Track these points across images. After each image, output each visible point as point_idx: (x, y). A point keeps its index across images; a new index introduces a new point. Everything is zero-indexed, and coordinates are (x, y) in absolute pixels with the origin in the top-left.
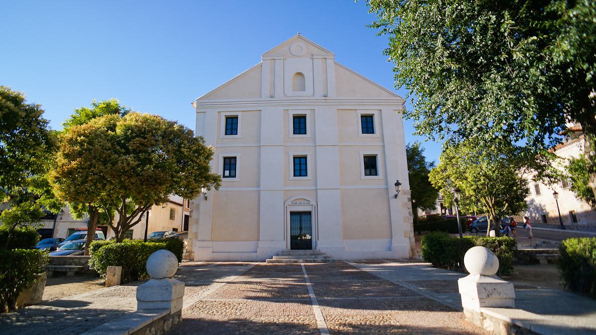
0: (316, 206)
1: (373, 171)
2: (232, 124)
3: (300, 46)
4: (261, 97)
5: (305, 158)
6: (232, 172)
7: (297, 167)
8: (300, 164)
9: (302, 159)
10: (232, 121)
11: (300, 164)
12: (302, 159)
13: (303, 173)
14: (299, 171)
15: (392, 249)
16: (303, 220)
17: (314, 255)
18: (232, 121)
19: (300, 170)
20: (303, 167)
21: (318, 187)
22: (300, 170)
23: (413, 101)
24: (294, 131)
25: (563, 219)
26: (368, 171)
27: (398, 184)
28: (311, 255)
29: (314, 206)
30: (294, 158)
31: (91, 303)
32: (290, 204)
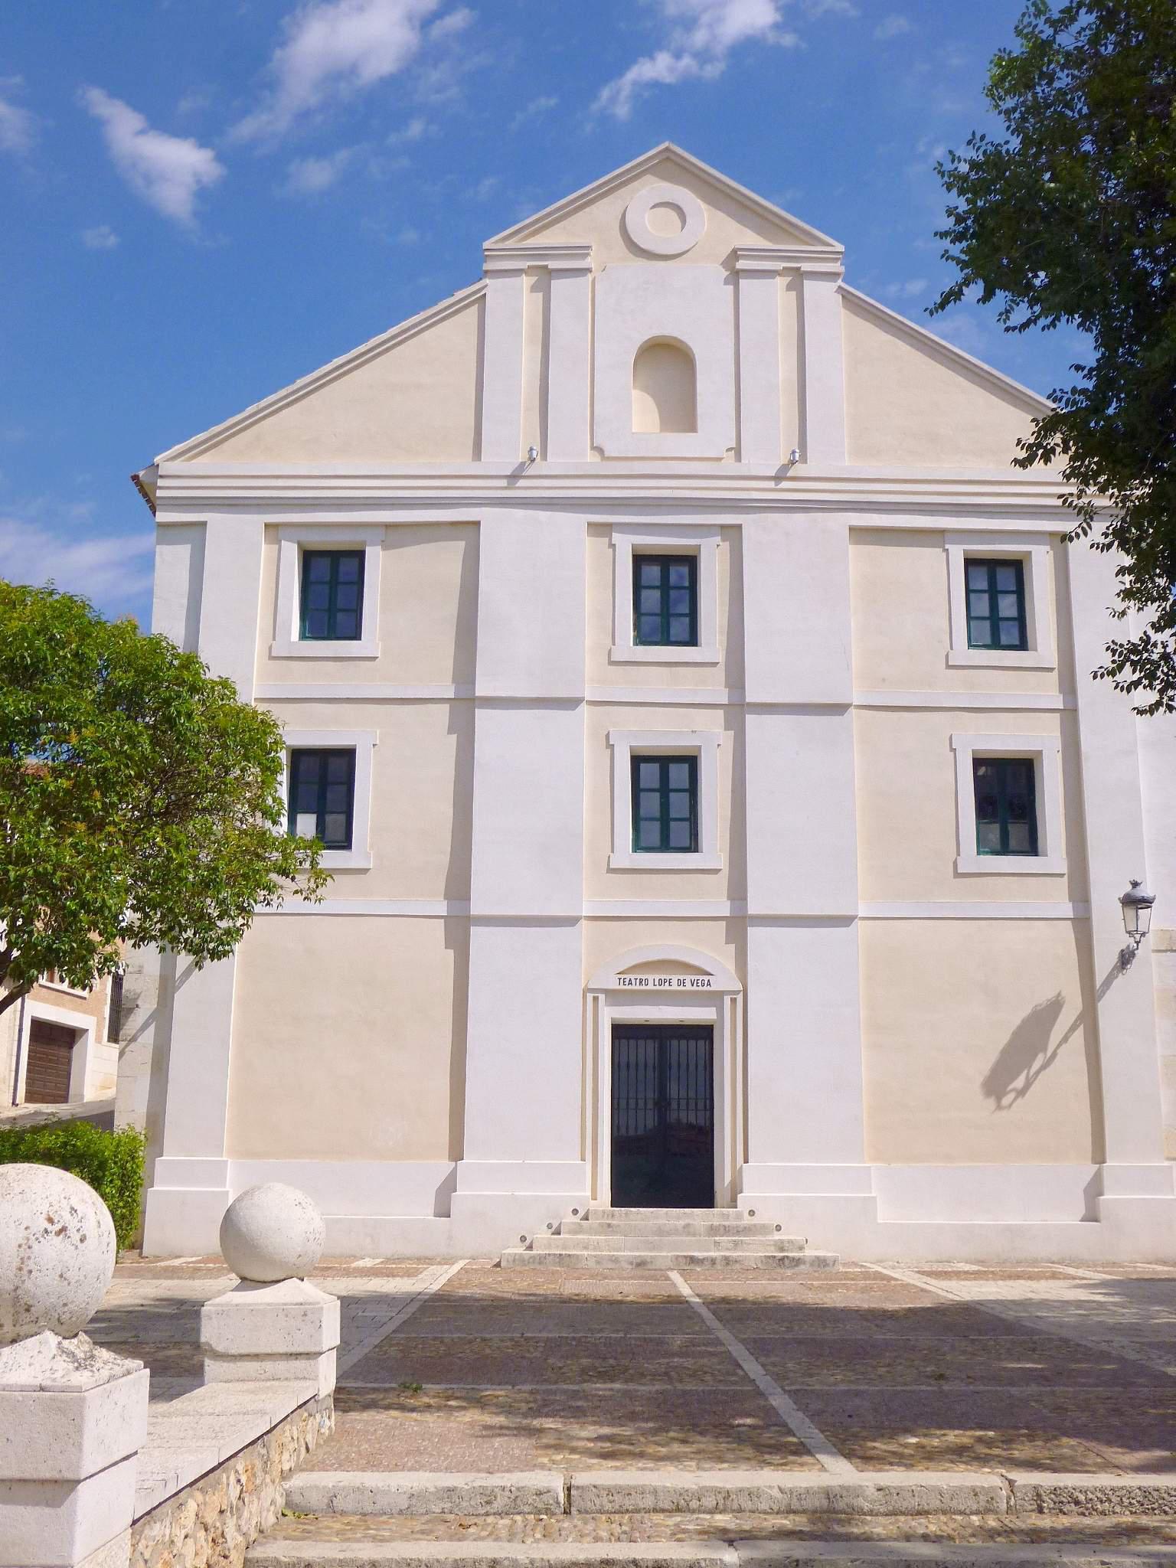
0: (740, 998)
1: (1017, 831)
2: (334, 583)
3: (636, 249)
4: (477, 453)
5: (691, 762)
6: (334, 820)
7: (652, 803)
8: (665, 790)
9: (673, 768)
10: (335, 570)
11: (665, 790)
12: (673, 768)
13: (678, 831)
14: (657, 825)
15: (1102, 1215)
16: (650, 1073)
17: (726, 1230)
18: (335, 570)
19: (665, 819)
20: (678, 803)
21: (754, 908)
22: (665, 819)
23: (73, 1247)
24: (637, 626)
25: (55, 1503)
26: (994, 832)
27: (1135, 902)
28: (713, 1230)
29: (727, 999)
30: (638, 761)
31: (683, 228)
32: (614, 985)
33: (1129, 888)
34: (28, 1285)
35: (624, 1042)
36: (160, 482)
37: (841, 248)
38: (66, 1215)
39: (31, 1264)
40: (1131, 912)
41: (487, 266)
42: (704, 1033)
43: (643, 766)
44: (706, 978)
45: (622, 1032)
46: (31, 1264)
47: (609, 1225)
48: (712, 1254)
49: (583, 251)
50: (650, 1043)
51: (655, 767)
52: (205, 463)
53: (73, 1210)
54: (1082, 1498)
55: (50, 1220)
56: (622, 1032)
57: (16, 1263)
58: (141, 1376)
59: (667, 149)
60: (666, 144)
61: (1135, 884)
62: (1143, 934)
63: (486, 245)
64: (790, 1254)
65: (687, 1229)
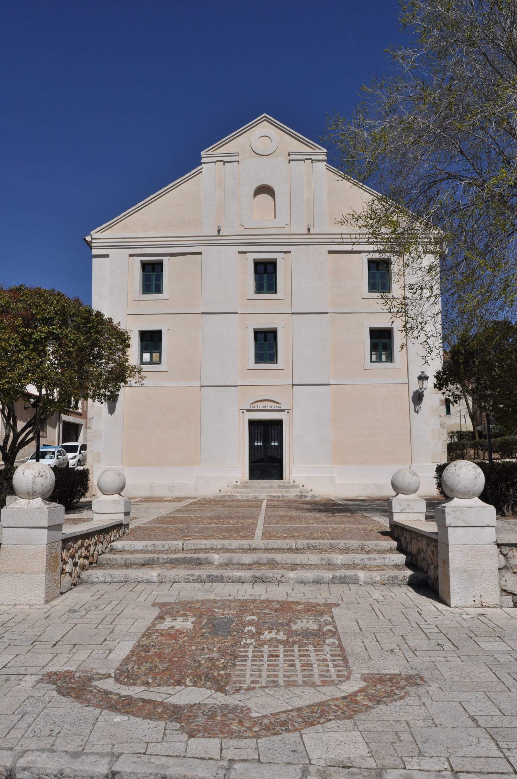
28: (280, 487)
32: (249, 408)
33: (421, 373)
34: (35, 487)
35: (253, 426)
36: (93, 241)
37: (325, 151)
38: (43, 473)
39: (35, 483)
40: (421, 382)
41: (202, 161)
42: (279, 423)
43: (258, 334)
44: (279, 405)
45: (252, 423)
46: (35, 483)
47: (246, 486)
48: (279, 494)
49: (237, 154)
50: (262, 427)
51: (263, 335)
52: (108, 234)
53: (44, 471)
54: (314, 545)
55: (39, 474)
56: (252, 423)
57: (32, 482)
58: (62, 508)
59: (265, 117)
60: (265, 114)
61: (423, 372)
62: (425, 389)
63: (202, 153)
64: (304, 494)
65: (271, 487)
